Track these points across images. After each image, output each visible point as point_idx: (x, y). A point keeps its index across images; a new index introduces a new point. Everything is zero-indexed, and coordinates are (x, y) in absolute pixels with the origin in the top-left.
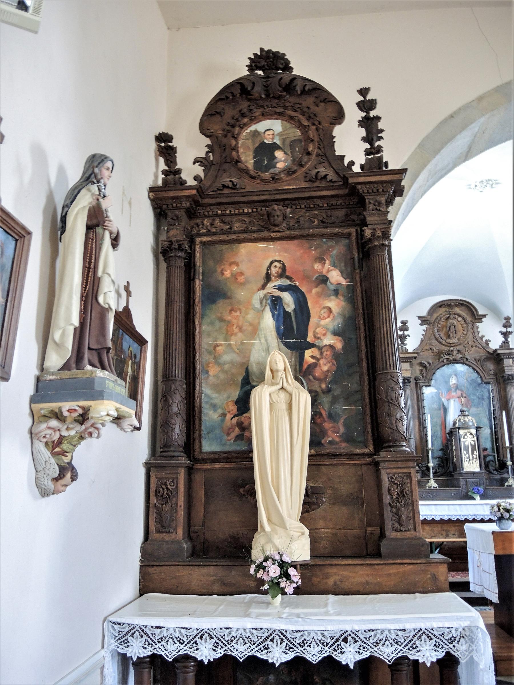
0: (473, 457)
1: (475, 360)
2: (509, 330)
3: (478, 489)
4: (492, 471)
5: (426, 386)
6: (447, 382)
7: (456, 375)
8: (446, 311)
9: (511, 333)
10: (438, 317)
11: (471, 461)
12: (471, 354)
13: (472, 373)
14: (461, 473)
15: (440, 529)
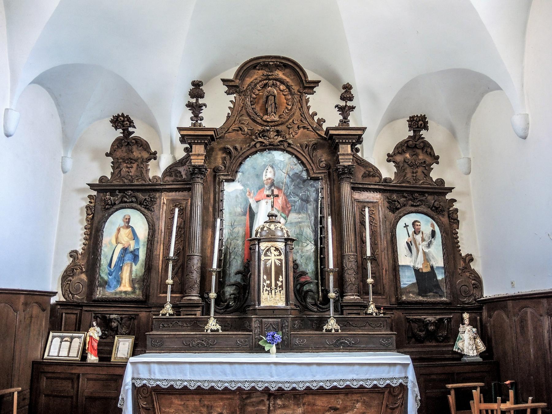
0: (276, 285)
1: (301, 146)
2: (349, 104)
3: (273, 336)
4: (310, 307)
5: (228, 181)
6: (258, 176)
7: (273, 167)
8: (263, 75)
9: (352, 108)
10: (252, 82)
11: (273, 292)
12: (299, 136)
13: (296, 165)
14: (255, 310)
15: (197, 403)
